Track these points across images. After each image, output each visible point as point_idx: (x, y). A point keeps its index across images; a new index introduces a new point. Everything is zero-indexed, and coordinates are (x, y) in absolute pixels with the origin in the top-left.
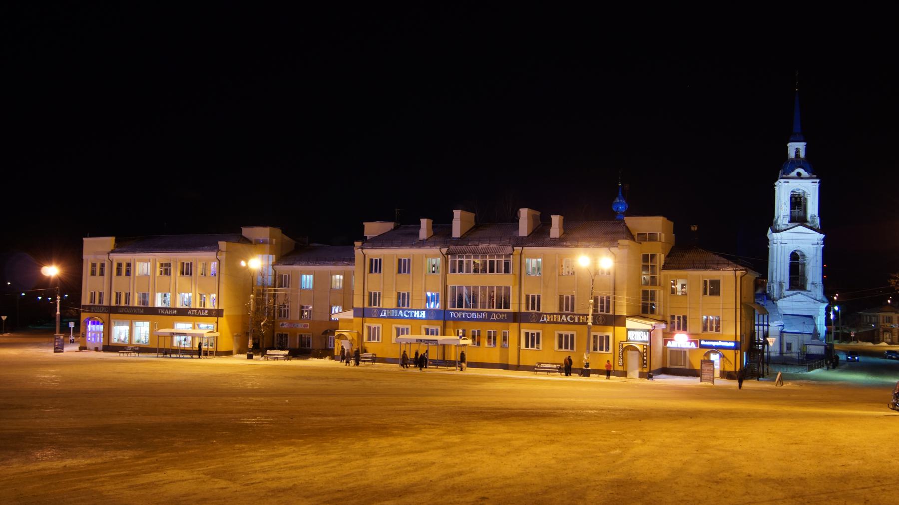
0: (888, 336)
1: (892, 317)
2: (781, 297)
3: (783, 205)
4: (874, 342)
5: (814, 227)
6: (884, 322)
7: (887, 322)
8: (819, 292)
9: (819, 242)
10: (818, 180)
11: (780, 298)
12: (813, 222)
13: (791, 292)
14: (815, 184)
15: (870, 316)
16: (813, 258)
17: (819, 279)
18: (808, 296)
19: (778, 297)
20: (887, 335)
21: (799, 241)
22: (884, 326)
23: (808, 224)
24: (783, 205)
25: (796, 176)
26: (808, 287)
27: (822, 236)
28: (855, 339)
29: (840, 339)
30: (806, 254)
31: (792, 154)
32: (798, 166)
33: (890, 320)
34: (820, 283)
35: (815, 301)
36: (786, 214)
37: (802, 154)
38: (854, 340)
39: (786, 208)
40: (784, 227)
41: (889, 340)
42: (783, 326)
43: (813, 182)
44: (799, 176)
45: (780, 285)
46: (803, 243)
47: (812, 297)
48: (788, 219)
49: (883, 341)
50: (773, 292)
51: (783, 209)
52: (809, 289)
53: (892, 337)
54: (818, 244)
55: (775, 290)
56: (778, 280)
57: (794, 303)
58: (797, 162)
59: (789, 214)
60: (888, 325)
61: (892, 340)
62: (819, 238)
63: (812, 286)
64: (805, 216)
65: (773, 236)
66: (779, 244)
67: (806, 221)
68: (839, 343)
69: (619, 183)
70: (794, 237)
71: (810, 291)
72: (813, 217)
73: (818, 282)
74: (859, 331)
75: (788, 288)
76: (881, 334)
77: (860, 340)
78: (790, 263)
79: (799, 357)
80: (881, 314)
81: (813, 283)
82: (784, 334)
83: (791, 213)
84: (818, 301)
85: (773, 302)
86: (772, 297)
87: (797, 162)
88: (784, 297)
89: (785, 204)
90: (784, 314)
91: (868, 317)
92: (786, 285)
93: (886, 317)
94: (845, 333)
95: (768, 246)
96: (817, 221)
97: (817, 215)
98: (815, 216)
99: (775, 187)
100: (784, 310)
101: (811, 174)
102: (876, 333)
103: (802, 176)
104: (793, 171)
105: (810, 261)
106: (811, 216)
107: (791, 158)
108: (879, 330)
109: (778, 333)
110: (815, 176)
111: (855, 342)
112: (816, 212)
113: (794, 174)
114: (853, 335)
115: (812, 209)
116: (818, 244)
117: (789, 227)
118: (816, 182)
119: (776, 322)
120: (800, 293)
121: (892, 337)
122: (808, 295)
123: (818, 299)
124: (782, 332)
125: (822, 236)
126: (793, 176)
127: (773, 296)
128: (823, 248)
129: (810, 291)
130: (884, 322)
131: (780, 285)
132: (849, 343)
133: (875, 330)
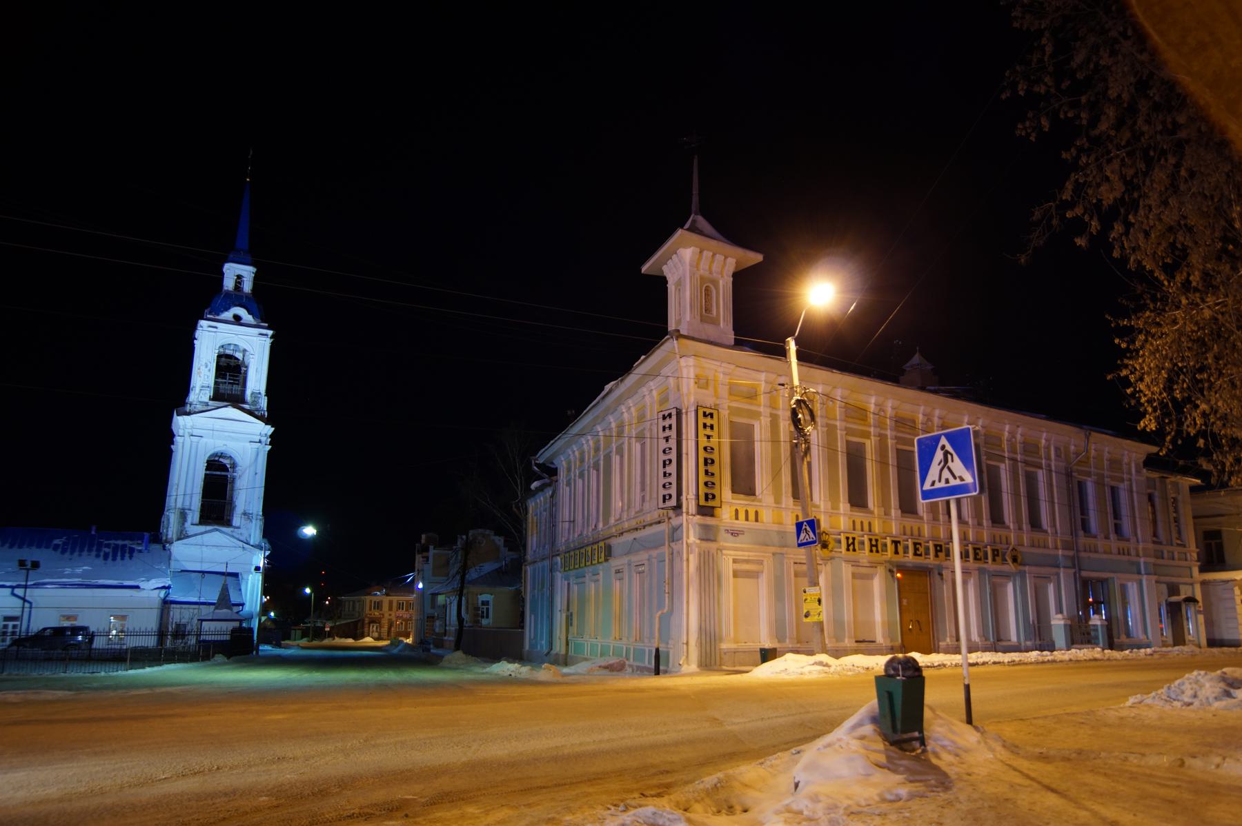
0: (375, 628)
1: (382, 601)
2: (182, 536)
3: (203, 368)
4: (356, 638)
5: (256, 413)
6: (370, 609)
7: (374, 608)
8: (254, 531)
9: (264, 439)
10: (270, 333)
11: (179, 539)
12: (255, 403)
13: (202, 528)
14: (263, 338)
15: (354, 602)
16: (250, 466)
17: (257, 507)
18: (233, 537)
19: (175, 537)
20: (374, 627)
21: (226, 434)
22: (371, 614)
23: (246, 406)
24: (203, 368)
25: (233, 320)
26: (236, 521)
27: (269, 430)
28: (330, 635)
29: (311, 635)
30: (238, 460)
31: (229, 284)
32: (237, 304)
33: (378, 605)
34: (257, 515)
35: (246, 546)
36: (206, 383)
37: (247, 287)
38: (329, 637)
39: (208, 373)
40: (200, 407)
41: (376, 635)
42: (168, 587)
43: (260, 334)
44: (237, 320)
45: (183, 515)
46: (233, 439)
47: (241, 538)
48: (210, 393)
49: (369, 636)
50: (167, 528)
51: (203, 375)
52: (238, 525)
53: (380, 630)
54: (260, 442)
55: (171, 525)
56: (179, 505)
57: (204, 549)
58: (236, 297)
59: (212, 385)
60: (376, 613)
61: (380, 633)
62: (263, 433)
63: (243, 516)
64: (244, 392)
65: (181, 423)
66: (187, 435)
67: (244, 402)
68: (309, 641)
69: (275, 615)
70: (217, 427)
71: (238, 528)
72: (256, 395)
73: (255, 513)
74: (337, 624)
75: (197, 519)
76: (367, 626)
77: (337, 636)
78: (206, 475)
79: (155, 635)
80: (368, 598)
81: (245, 514)
82: (173, 606)
83: (216, 383)
84: (252, 546)
85: (164, 547)
86: (164, 538)
87: (236, 297)
88: (188, 537)
89: (206, 367)
90: (182, 571)
91: (351, 603)
92: (194, 516)
93: (375, 602)
94: (318, 627)
95: (172, 446)
96: (264, 403)
97: (263, 392)
98: (260, 393)
99: (195, 341)
100: (184, 563)
101: (260, 321)
102: (359, 624)
103: (242, 321)
104: (227, 309)
105: (246, 470)
106: (253, 393)
107: (228, 290)
108: (363, 620)
109: (157, 603)
110: (267, 325)
111: (330, 639)
112: (262, 387)
113: (228, 315)
114: (327, 629)
115: (257, 380)
116: (260, 442)
117: (209, 408)
118: (266, 335)
119: (153, 581)
120: (217, 530)
121: (380, 630)
122: (234, 534)
123: (252, 543)
124: (166, 603)
125: (269, 430)
126: (224, 319)
127: (167, 535)
128: (270, 452)
129: (238, 528)
130: (370, 609)
131: (183, 515)
132: (322, 640)
133: (359, 621)
